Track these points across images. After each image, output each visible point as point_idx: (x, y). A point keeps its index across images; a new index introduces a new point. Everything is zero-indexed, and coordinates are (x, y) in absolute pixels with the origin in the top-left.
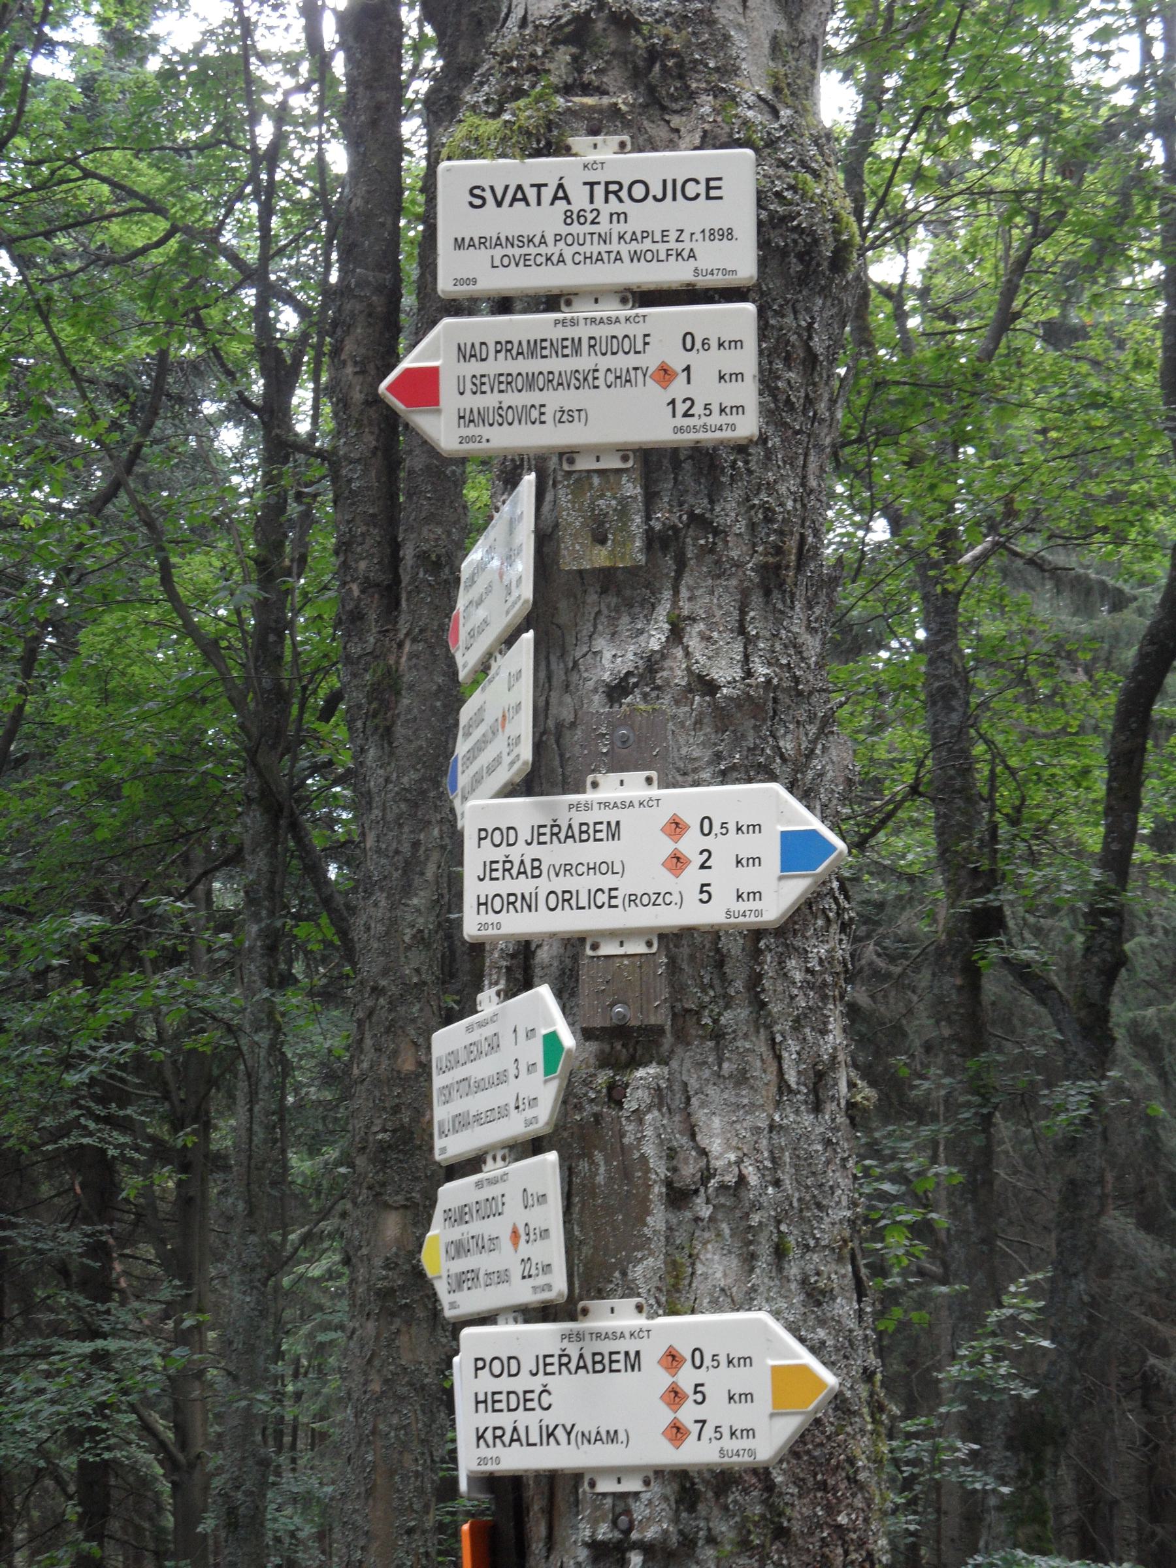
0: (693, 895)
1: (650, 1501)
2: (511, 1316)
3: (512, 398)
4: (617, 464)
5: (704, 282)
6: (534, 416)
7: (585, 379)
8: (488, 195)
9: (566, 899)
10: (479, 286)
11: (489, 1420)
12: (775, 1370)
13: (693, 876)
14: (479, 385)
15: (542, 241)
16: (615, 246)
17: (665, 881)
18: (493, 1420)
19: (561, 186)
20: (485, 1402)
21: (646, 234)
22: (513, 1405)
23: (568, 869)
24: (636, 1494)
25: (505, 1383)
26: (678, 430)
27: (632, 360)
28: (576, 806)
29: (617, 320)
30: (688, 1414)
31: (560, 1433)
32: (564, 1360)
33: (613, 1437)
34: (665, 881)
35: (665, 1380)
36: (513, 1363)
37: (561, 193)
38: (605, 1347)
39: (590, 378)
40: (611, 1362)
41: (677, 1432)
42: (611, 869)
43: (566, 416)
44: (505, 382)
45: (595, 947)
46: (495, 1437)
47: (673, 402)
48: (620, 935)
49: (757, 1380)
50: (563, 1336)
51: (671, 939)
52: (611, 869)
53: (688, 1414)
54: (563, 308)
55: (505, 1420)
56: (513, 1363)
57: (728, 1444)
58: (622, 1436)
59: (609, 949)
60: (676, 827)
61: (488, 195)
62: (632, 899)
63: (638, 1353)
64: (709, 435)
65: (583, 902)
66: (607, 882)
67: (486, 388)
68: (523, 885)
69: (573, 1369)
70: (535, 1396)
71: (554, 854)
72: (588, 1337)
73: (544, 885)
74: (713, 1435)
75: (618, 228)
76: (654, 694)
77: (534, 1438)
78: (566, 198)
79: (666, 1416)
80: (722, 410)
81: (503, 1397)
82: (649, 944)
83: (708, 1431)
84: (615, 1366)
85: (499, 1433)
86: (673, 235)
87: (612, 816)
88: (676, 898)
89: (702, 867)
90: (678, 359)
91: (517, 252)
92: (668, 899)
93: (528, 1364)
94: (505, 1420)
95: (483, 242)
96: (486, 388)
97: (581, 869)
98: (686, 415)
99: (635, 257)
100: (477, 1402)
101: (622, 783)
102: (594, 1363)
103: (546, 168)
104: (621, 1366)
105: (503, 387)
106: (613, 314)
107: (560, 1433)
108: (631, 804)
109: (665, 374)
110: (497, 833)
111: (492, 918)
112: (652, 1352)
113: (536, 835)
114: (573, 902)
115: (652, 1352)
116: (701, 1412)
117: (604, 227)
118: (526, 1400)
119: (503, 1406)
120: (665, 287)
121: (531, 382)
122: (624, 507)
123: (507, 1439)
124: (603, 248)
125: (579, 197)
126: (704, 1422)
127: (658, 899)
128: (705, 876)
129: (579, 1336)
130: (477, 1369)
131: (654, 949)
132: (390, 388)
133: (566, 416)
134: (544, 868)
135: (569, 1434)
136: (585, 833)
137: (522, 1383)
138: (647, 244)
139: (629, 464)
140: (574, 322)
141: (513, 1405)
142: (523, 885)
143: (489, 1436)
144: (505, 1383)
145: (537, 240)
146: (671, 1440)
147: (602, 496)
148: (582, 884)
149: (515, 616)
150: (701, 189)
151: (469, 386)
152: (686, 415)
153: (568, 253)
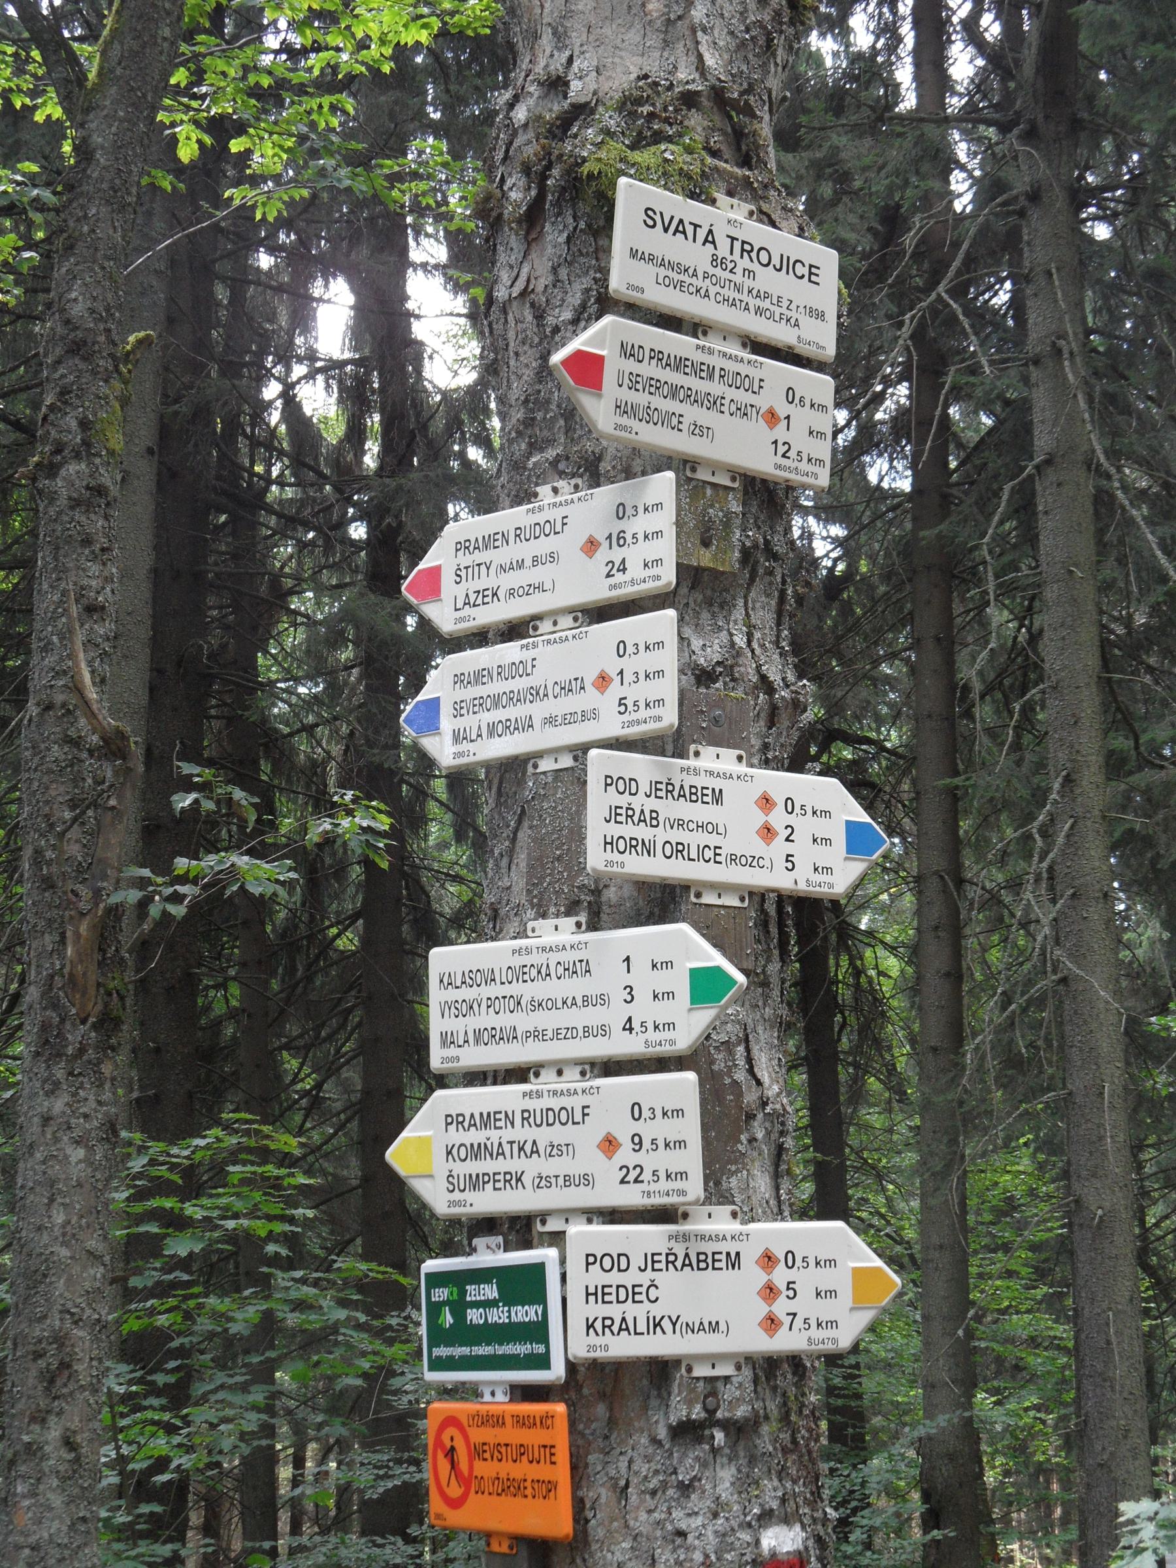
0: (780, 863)
1: (741, 1384)
2: (584, 1218)
3: (658, 402)
4: (727, 482)
5: (803, 350)
6: (672, 421)
8: (658, 218)
9: (679, 850)
10: (645, 296)
11: (598, 1310)
12: (856, 1271)
13: (779, 847)
14: (635, 382)
15: (695, 275)
16: (744, 297)
17: (757, 847)
18: (601, 1310)
19: (710, 232)
20: (596, 1294)
21: (767, 296)
22: (622, 1297)
23: (681, 824)
24: (727, 1379)
25: (615, 1278)
26: (778, 467)
27: (749, 398)
28: (687, 770)
29: (742, 361)
30: (781, 1307)
31: (666, 1324)
32: (671, 1258)
33: (714, 1327)
34: (757, 847)
35: (762, 1278)
36: (623, 1259)
37: (710, 239)
38: (709, 1247)
40: (714, 1261)
41: (771, 1323)
42: (715, 830)
43: (698, 430)
44: (655, 386)
45: (698, 895)
46: (604, 1327)
47: (776, 442)
48: (720, 888)
49: (842, 1280)
50: (670, 1237)
51: (758, 896)
52: (715, 830)
53: (781, 1307)
55: (615, 1311)
56: (623, 1259)
57: (815, 1333)
58: (723, 1327)
59: (709, 899)
60: (766, 802)
61: (658, 218)
62: (733, 858)
63: (738, 1254)
64: (799, 478)
65: (694, 855)
66: (713, 840)
68: (643, 832)
70: (643, 1289)
71: (670, 808)
72: (693, 1238)
73: (661, 835)
74: (802, 1326)
75: (748, 283)
76: (731, 685)
77: (641, 1327)
78: (713, 242)
79: (762, 1309)
81: (613, 1290)
82: (742, 899)
83: (798, 1323)
84: (717, 1265)
85: (608, 1322)
86: (785, 304)
87: (717, 784)
88: (767, 863)
89: (787, 840)
90: (782, 409)
91: (676, 277)
92: (761, 862)
93: (637, 1261)
94: (615, 1311)
95: (651, 259)
96: (639, 386)
97: (692, 826)
98: (784, 456)
99: (759, 311)
100: (588, 1294)
102: (699, 1261)
103: (693, 211)
104: (723, 1264)
105: (652, 390)
106: (734, 352)
107: (666, 1324)
108: (731, 777)
109: (772, 417)
110: (621, 782)
111: (616, 857)
112: (750, 1254)
113: (655, 789)
114: (685, 853)
115: (750, 1254)
116: (792, 1306)
117: (738, 278)
118: (634, 1294)
119: (613, 1298)
120: (773, 343)
121: (674, 392)
122: (729, 520)
123: (615, 1328)
124: (737, 296)
125: (723, 249)
126: (795, 1315)
127: (753, 862)
128: (789, 848)
129: (685, 1237)
130: (588, 1264)
131: (746, 904)
132: (566, 362)
133: (698, 430)
134: (661, 819)
135: (674, 1325)
136: (694, 795)
137: (630, 1278)
138: (766, 304)
139: (736, 485)
140: (711, 352)
141: (622, 1297)
142: (643, 832)
143: (598, 1325)
144: (615, 1278)
145: (691, 271)
146: (766, 1330)
147: (712, 506)
148: (694, 839)
149: (618, 597)
150: (806, 271)
151: (626, 381)
152: (784, 456)
153: (713, 290)
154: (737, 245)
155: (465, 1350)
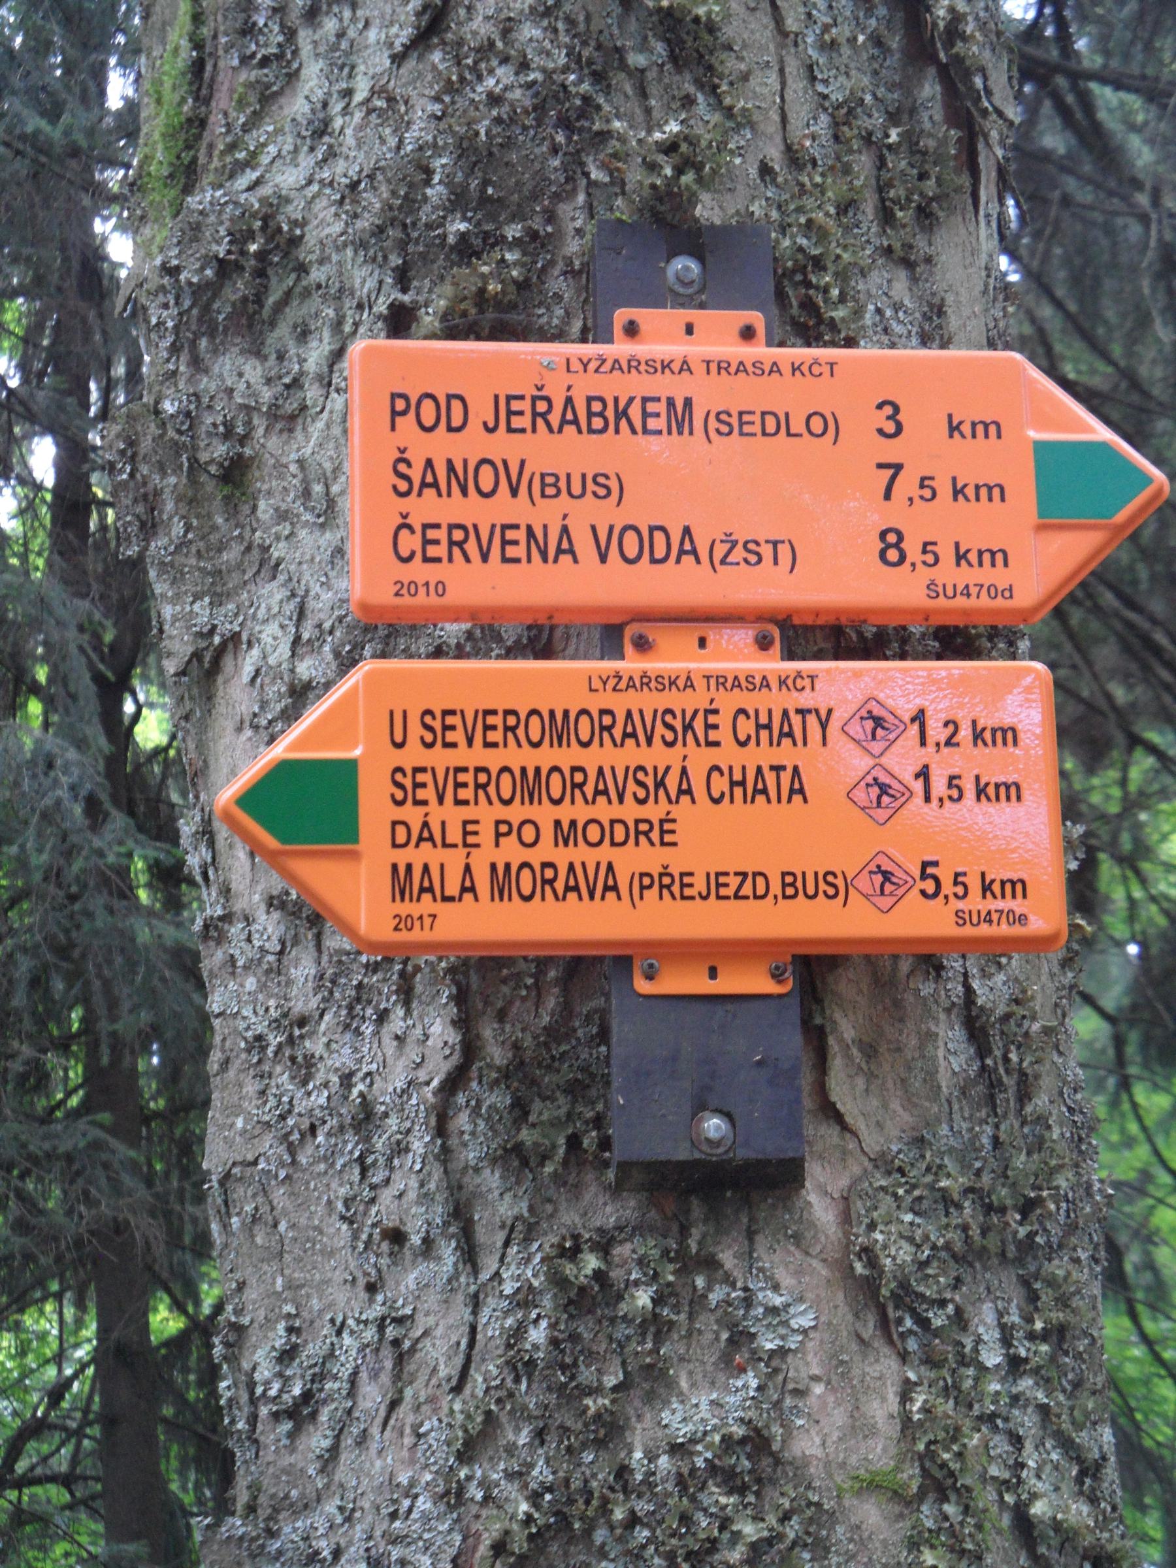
7: (688, 727)
22: (771, 428)
36: (456, 405)
39: (699, 725)
54: (629, 649)
56: (456, 405)
67: (457, 736)
69: (555, 425)
74: (916, 492)
80: (986, 888)
101: (689, 330)
102: (590, 414)
119: (757, 428)
141: (771, 428)
151: (416, 730)
154: (713, 682)
155: (1092, 521)
